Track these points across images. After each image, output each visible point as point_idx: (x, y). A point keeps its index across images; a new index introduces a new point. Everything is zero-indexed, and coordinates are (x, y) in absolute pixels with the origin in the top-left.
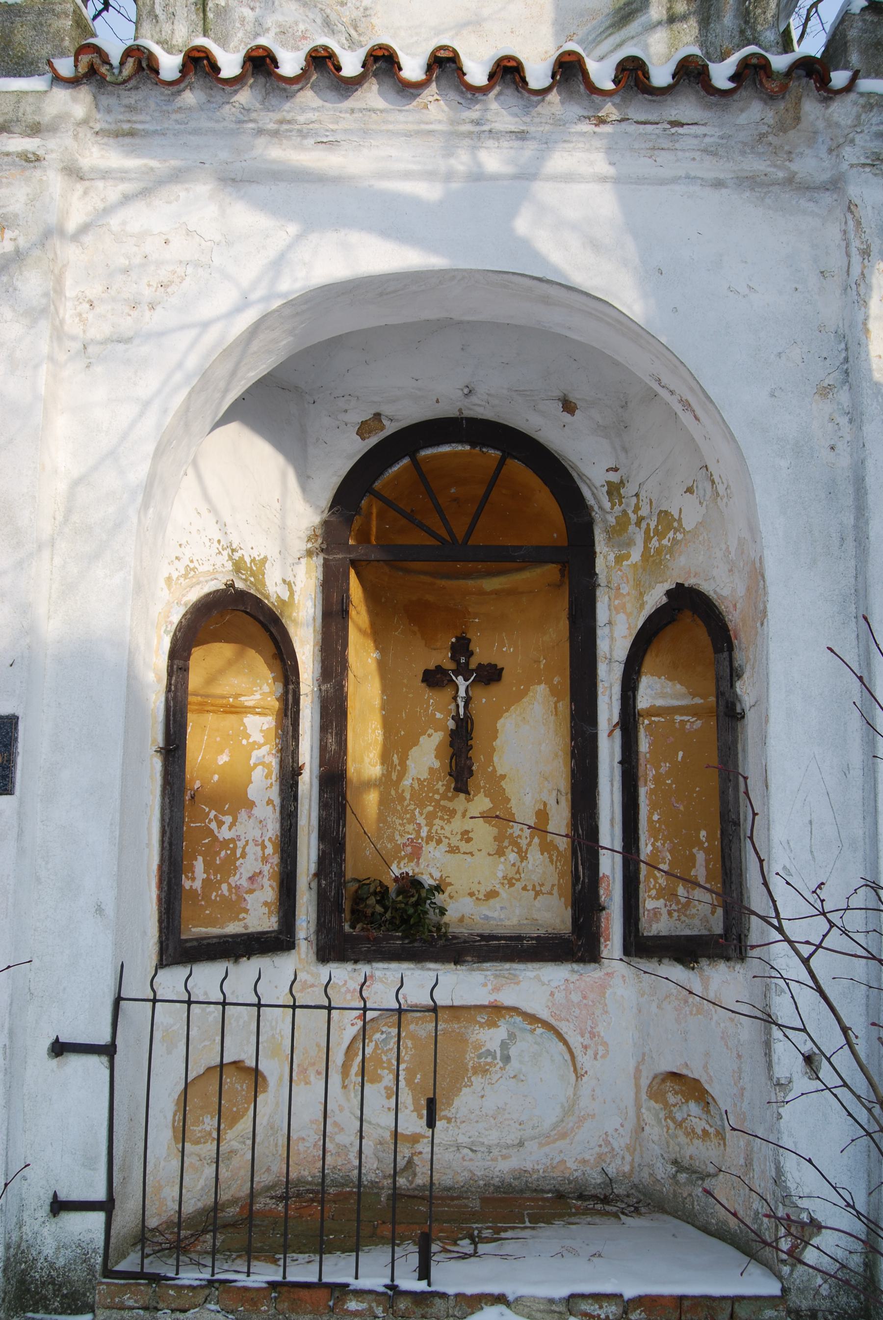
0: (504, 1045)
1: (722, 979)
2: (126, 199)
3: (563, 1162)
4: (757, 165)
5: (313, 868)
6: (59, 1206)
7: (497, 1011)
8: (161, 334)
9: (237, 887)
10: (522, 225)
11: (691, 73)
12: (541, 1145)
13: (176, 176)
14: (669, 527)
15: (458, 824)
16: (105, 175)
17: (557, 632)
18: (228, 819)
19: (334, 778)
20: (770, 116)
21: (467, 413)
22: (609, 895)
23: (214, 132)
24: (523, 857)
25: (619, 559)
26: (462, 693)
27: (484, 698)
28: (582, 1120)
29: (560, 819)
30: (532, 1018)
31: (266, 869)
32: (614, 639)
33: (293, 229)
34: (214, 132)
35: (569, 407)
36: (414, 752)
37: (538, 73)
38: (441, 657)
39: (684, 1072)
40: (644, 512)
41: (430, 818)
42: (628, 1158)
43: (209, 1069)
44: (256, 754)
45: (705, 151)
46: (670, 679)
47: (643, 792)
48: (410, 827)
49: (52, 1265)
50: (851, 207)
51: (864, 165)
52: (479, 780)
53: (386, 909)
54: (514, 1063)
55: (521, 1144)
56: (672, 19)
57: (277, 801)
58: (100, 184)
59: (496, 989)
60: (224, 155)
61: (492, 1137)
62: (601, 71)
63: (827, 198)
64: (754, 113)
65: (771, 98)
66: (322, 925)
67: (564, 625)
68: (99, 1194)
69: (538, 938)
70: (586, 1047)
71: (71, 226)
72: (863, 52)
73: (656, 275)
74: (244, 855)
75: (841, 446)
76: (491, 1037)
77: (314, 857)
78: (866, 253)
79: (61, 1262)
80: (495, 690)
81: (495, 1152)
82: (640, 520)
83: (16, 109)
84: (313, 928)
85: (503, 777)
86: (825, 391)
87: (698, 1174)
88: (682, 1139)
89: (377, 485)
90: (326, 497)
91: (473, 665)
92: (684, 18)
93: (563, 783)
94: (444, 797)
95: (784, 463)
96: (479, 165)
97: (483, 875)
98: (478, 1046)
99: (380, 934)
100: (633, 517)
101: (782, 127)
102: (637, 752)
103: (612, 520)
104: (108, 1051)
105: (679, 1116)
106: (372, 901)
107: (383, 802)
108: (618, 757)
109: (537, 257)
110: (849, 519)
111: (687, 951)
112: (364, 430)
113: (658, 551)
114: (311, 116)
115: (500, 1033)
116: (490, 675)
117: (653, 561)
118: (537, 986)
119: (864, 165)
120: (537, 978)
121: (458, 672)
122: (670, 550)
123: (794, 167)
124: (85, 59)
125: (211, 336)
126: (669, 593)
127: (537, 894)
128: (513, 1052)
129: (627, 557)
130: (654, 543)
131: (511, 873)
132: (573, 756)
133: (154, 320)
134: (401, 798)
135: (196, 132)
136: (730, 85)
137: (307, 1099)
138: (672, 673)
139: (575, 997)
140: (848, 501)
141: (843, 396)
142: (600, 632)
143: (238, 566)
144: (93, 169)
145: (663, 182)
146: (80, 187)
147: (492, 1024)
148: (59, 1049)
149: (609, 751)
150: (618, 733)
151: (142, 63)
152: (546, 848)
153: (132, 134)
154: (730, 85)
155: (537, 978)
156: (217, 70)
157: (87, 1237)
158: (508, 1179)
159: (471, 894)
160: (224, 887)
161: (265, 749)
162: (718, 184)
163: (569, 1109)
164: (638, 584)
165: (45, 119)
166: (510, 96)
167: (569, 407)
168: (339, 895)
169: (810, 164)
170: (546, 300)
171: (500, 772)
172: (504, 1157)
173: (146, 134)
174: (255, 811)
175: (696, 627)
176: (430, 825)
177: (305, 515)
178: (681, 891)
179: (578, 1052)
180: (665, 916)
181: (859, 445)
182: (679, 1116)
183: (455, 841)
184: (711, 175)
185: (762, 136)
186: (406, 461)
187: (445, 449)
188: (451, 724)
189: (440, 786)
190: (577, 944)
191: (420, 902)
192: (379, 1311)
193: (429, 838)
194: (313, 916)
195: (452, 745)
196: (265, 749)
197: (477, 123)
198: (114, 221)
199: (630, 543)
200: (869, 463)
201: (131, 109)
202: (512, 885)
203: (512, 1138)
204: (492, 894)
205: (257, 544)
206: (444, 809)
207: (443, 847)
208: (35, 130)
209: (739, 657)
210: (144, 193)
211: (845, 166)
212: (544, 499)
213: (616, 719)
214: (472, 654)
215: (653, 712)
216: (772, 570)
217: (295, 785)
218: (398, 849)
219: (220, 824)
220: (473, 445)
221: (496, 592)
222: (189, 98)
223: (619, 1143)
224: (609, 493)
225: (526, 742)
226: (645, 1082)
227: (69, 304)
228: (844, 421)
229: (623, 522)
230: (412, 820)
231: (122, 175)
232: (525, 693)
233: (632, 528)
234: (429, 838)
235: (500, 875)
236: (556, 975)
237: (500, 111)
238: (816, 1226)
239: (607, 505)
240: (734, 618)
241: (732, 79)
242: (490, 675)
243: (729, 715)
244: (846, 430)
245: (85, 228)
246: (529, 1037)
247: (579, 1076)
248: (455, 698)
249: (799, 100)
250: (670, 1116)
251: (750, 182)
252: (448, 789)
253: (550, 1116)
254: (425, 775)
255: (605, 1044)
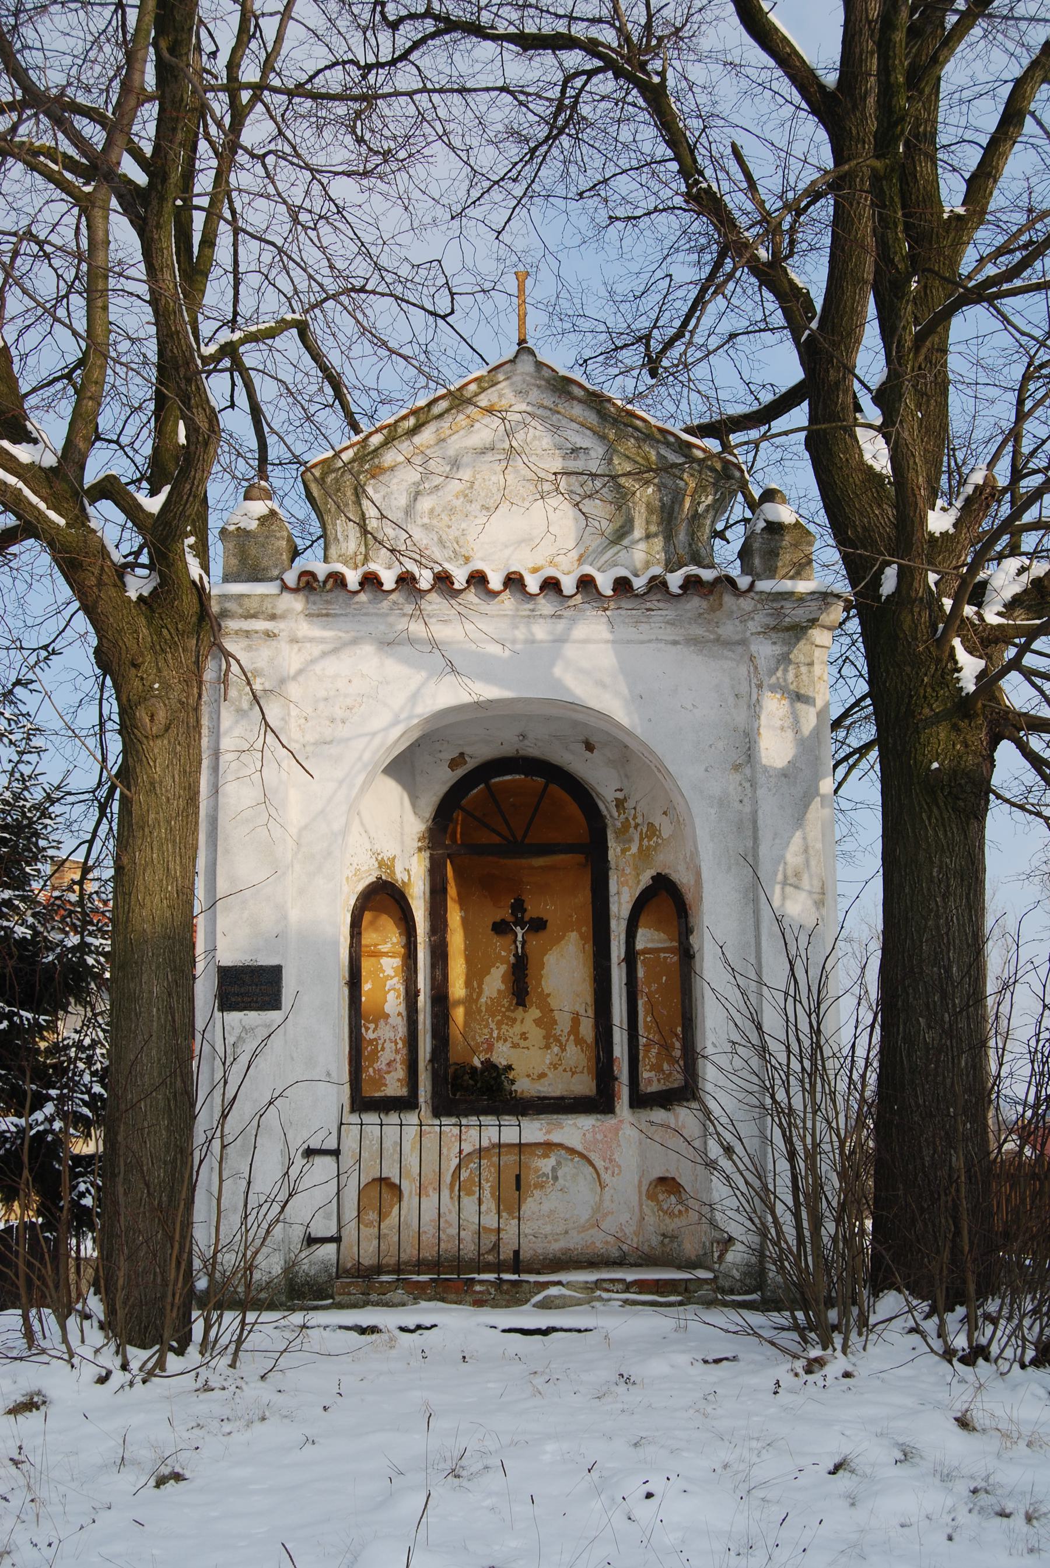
0: (554, 1169)
1: (684, 1116)
2: (324, 654)
3: (593, 1243)
4: (698, 631)
5: (428, 1056)
6: (311, 1241)
7: (549, 1146)
8: (348, 739)
9: (379, 1070)
10: (558, 671)
11: (657, 585)
12: (579, 1232)
13: (355, 642)
14: (654, 834)
15: (518, 1029)
16: (311, 640)
17: (584, 897)
18: (372, 1026)
19: (440, 998)
20: (705, 604)
21: (522, 753)
22: (620, 1070)
23: (376, 614)
24: (563, 1049)
25: (624, 851)
26: (520, 938)
27: (535, 942)
28: (606, 1215)
29: (587, 1029)
30: (572, 1151)
31: (398, 1057)
32: (621, 902)
33: (424, 674)
34: (376, 614)
35: (589, 747)
36: (487, 979)
37: (568, 585)
38: (504, 913)
39: (667, 1175)
40: (639, 820)
41: (499, 1024)
42: (635, 1240)
43: (374, 1180)
44: (389, 983)
45: (667, 623)
46: (657, 930)
47: (640, 1003)
48: (486, 1031)
49: (307, 1275)
50: (752, 658)
51: (759, 633)
52: (533, 997)
53: (476, 1082)
54: (561, 1181)
55: (566, 1232)
56: (648, 536)
57: (404, 1014)
58: (308, 645)
59: (548, 1132)
60: (382, 628)
61: (547, 1229)
62: (604, 583)
63: (740, 649)
64: (695, 603)
65: (704, 596)
66: (435, 1094)
67: (588, 893)
68: (332, 1231)
69: (575, 1098)
70: (607, 1169)
71: (292, 672)
72: (762, 558)
73: (638, 700)
74: (383, 1049)
75: (745, 800)
76: (546, 1164)
77: (429, 1048)
78: (760, 686)
79: (313, 1272)
80: (543, 936)
81: (550, 1238)
82: (637, 826)
83: (261, 606)
84: (429, 1095)
85: (549, 995)
86: (737, 767)
87: (673, 1238)
88: (668, 1221)
89: (463, 802)
90: (429, 811)
91: (526, 919)
92: (656, 535)
93: (589, 998)
94: (508, 1009)
95: (713, 811)
96: (532, 634)
97: (533, 1060)
98: (537, 1170)
99: (473, 1097)
100: (632, 823)
101: (712, 609)
102: (636, 977)
103: (619, 824)
104: (336, 1153)
105: (665, 1207)
106: (467, 1077)
107: (467, 1014)
108: (624, 981)
109: (568, 690)
110: (750, 844)
111: (666, 1099)
112: (453, 764)
113: (648, 848)
114: (435, 607)
115: (552, 1161)
116: (538, 925)
117: (645, 855)
118: (574, 1130)
119: (759, 633)
120: (575, 1124)
121: (517, 923)
122: (655, 849)
123: (720, 631)
124: (304, 579)
125: (377, 741)
126: (653, 878)
127: (573, 1073)
128: (560, 1173)
129: (629, 849)
130: (645, 842)
131: (556, 1060)
132: (595, 980)
133: (342, 731)
134: (479, 1011)
135: (365, 614)
136: (680, 592)
137: (430, 1204)
138: (658, 926)
139: (599, 1137)
140: (750, 833)
141: (748, 771)
142: (611, 900)
143: (381, 864)
144: (305, 637)
145: (642, 642)
146: (296, 647)
147: (546, 1156)
148: (310, 1153)
149: (618, 976)
150: (624, 964)
151: (338, 580)
152: (579, 1041)
153: (327, 615)
154: (680, 592)
155: (575, 1124)
156: (382, 584)
157: (327, 1258)
158: (559, 1254)
159: (528, 1076)
160: (371, 1070)
161: (396, 979)
162: (675, 643)
163: (597, 1208)
164: (636, 868)
165: (278, 612)
166: (552, 596)
167: (589, 747)
168: (446, 1073)
169: (729, 629)
170: (575, 711)
171: (546, 991)
172: (556, 1240)
173: (336, 615)
174: (390, 1020)
175: (668, 901)
176: (499, 1029)
177: (415, 826)
178: (666, 1066)
179: (602, 1172)
180: (655, 1082)
181: (755, 801)
182: (665, 1207)
183: (516, 1040)
184: (671, 638)
185: (700, 614)
186: (482, 786)
187: (508, 777)
188: (512, 959)
189: (505, 1002)
190: (599, 1103)
191: (499, 1076)
192: (492, 1291)
193: (499, 1038)
194: (429, 1088)
195: (513, 974)
196: (396, 979)
197: (533, 610)
198: (318, 668)
199: (631, 840)
200: (760, 813)
201: (327, 602)
202: (556, 1068)
203: (560, 1229)
204: (542, 1076)
205: (389, 848)
206: (508, 1018)
207: (508, 1044)
208: (273, 617)
209: (692, 921)
210: (335, 651)
211: (748, 634)
212: (573, 809)
213: (623, 956)
214: (525, 910)
215: (646, 951)
216: (705, 875)
217: (416, 1002)
218: (478, 1045)
219: (367, 1029)
220: (526, 775)
221: (541, 867)
222: (363, 597)
223: (629, 1230)
224: (617, 806)
225: (564, 972)
226: (644, 1188)
227: (293, 720)
228: (747, 785)
229: (626, 825)
230: (487, 1026)
231: (322, 640)
232: (563, 938)
233: (632, 830)
234: (499, 1038)
235: (548, 1062)
236: (586, 1122)
237: (546, 605)
238: (731, 1240)
239: (616, 814)
240: (689, 897)
241: (680, 587)
242: (538, 925)
243: (687, 956)
244: (749, 790)
245: (300, 672)
246: (570, 1164)
247: (602, 1186)
248: (515, 942)
249: (721, 597)
250: (661, 1209)
251: (694, 642)
252: (511, 1004)
253: (584, 1215)
254: (495, 995)
255: (619, 1166)
